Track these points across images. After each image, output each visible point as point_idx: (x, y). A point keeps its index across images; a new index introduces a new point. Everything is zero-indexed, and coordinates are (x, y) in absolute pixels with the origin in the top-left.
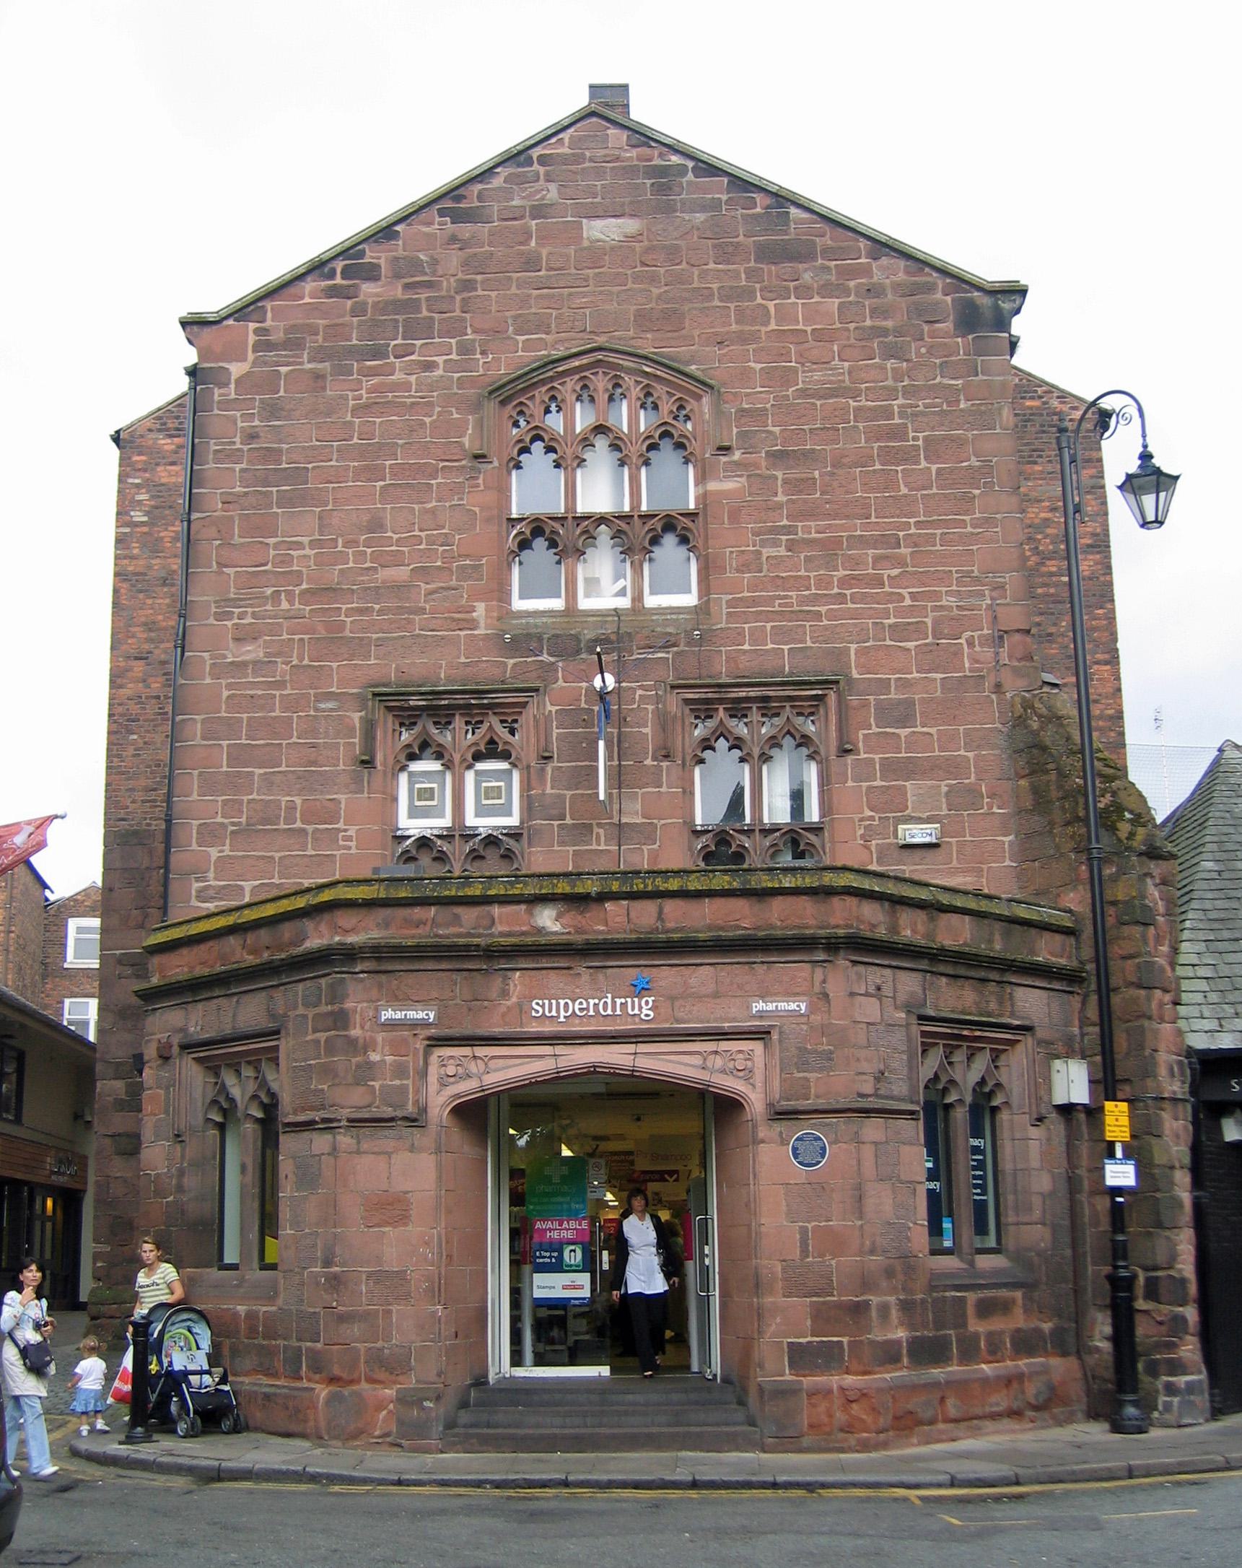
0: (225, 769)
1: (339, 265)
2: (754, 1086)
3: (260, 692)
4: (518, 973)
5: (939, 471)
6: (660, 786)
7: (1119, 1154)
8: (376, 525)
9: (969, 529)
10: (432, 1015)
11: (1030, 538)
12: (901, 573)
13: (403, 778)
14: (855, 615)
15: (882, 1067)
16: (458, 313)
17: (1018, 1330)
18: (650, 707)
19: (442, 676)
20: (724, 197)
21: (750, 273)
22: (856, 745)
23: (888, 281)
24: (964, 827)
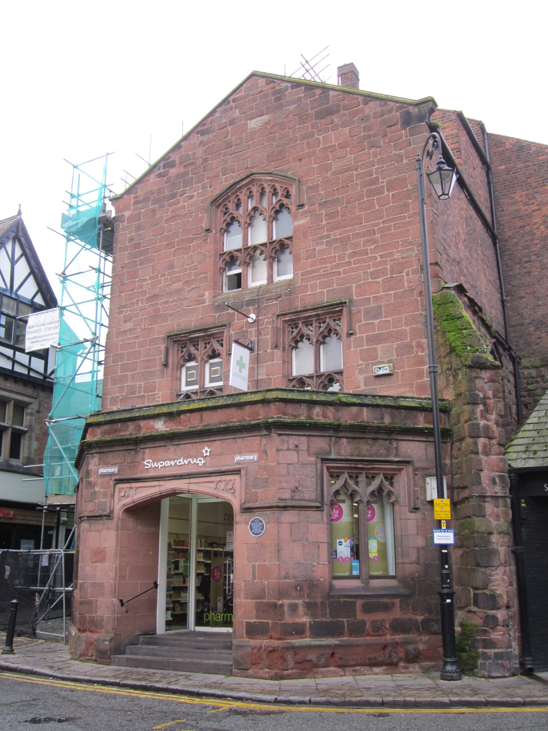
0: (119, 374)
1: (161, 165)
2: (235, 496)
3: (131, 341)
4: (147, 450)
5: (393, 195)
6: (273, 361)
7: (444, 527)
8: (171, 266)
9: (407, 219)
10: (116, 470)
11: (544, 222)
12: (376, 247)
13: (184, 370)
14: (356, 270)
15: (297, 485)
16: (202, 172)
17: (396, 620)
18: (270, 326)
19: (193, 325)
20: (303, 95)
21: (313, 126)
22: (355, 331)
23: (371, 113)
24: (404, 364)
